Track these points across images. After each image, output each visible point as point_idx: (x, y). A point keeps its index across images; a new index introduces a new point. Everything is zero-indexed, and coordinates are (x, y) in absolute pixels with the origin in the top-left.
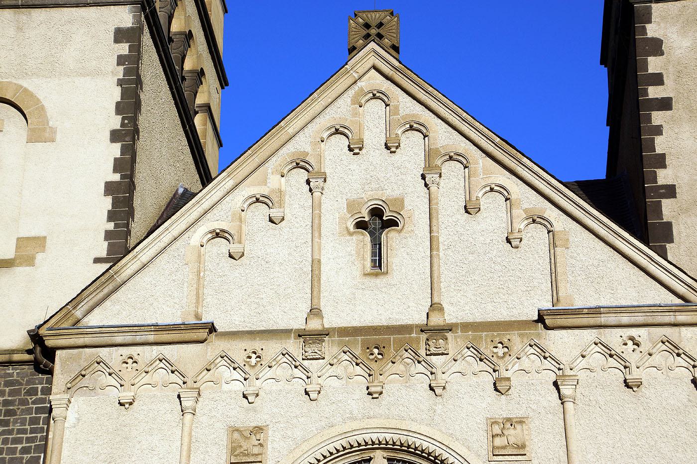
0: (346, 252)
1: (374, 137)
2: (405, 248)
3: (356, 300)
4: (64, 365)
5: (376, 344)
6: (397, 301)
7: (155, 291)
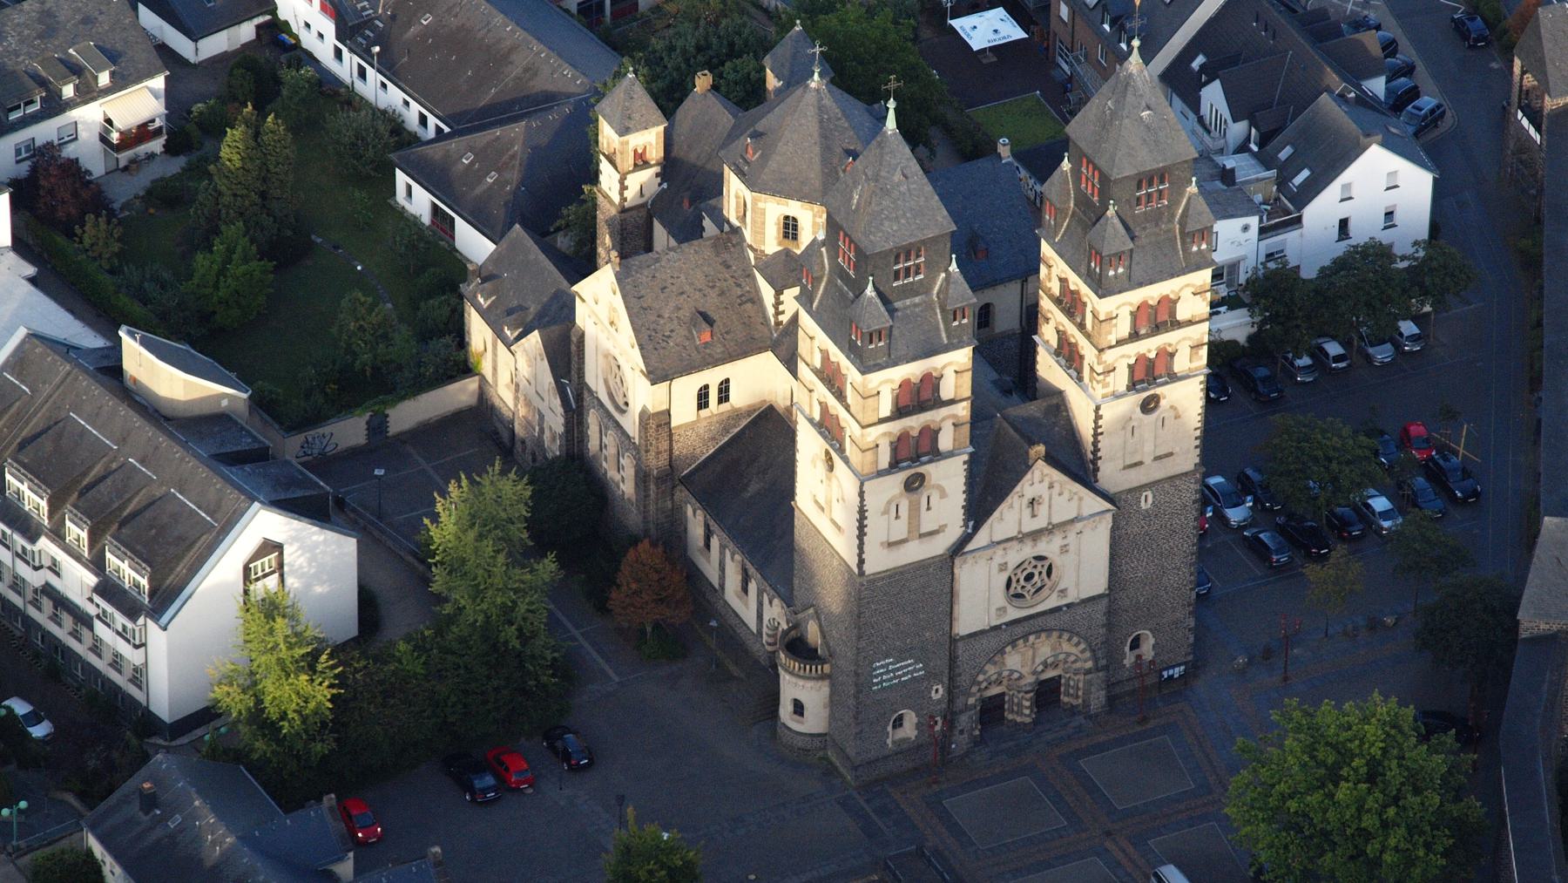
0: (1027, 512)
2: (1042, 510)
3: (1030, 525)
4: (957, 561)
5: (1035, 535)
6: (1040, 523)
7: (981, 538)
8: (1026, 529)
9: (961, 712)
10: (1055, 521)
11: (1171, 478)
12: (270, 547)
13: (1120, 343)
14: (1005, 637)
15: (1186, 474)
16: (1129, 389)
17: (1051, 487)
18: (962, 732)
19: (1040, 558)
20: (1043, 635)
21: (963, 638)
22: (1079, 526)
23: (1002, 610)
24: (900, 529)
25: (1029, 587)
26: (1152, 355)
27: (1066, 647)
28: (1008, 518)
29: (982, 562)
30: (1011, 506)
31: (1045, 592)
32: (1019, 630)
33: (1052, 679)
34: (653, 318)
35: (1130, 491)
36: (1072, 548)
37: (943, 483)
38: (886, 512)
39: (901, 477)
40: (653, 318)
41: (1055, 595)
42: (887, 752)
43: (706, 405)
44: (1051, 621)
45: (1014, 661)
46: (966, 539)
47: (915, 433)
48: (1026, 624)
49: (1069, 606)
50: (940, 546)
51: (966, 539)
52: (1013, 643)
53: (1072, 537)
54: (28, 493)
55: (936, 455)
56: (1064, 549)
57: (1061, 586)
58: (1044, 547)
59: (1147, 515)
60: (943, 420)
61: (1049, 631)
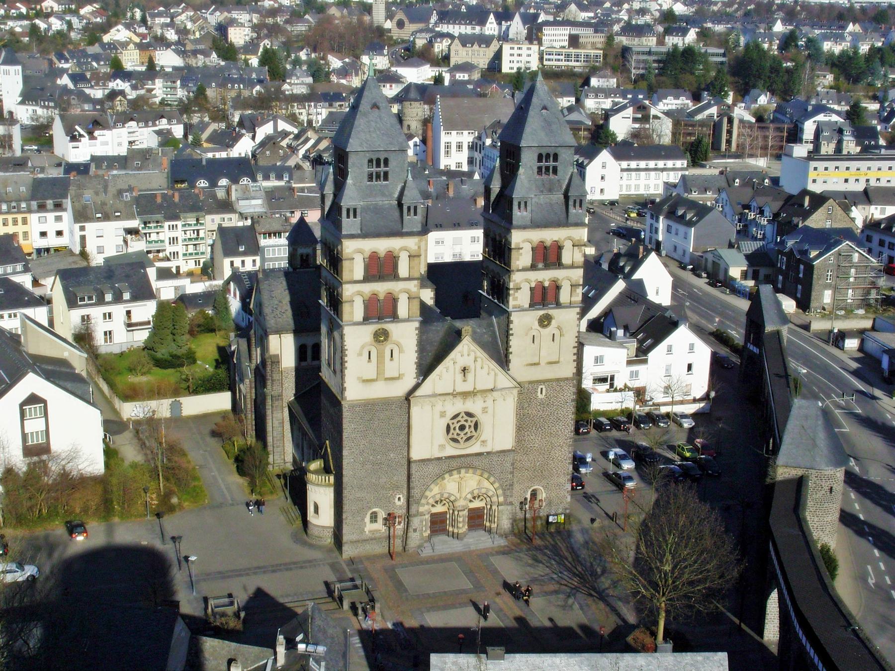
0: (459, 376)
1: (465, 353)
2: (470, 376)
3: (462, 387)
5: (465, 395)
6: (468, 387)
7: (427, 387)
8: (459, 390)
9: (415, 516)
10: (479, 388)
11: (558, 380)
12: (34, 399)
13: (524, 269)
14: (445, 466)
15: (567, 379)
16: (531, 306)
17: (475, 361)
18: (415, 530)
19: (469, 415)
20: (471, 471)
21: (415, 461)
22: (495, 394)
23: (442, 447)
24: (370, 371)
25: (462, 434)
26: (548, 244)
27: (486, 484)
28: (445, 375)
29: (428, 408)
30: (440, 377)
31: (473, 441)
32: (454, 464)
33: (478, 509)
34: (276, 302)
35: (530, 382)
36: (490, 411)
37: (401, 341)
38: (360, 354)
39: (371, 328)
40: (276, 302)
41: (479, 443)
42: (364, 537)
43: (305, 360)
44: (476, 462)
45: (451, 485)
46: (417, 386)
47: (381, 297)
48: (459, 460)
49: (488, 453)
50: (399, 390)
51: (417, 386)
52: (450, 472)
53: (489, 402)
54: (563, 549)
55: (394, 316)
56: (485, 411)
57: (482, 438)
58: (474, 406)
59: (542, 403)
60: (401, 291)
61: (475, 468)
